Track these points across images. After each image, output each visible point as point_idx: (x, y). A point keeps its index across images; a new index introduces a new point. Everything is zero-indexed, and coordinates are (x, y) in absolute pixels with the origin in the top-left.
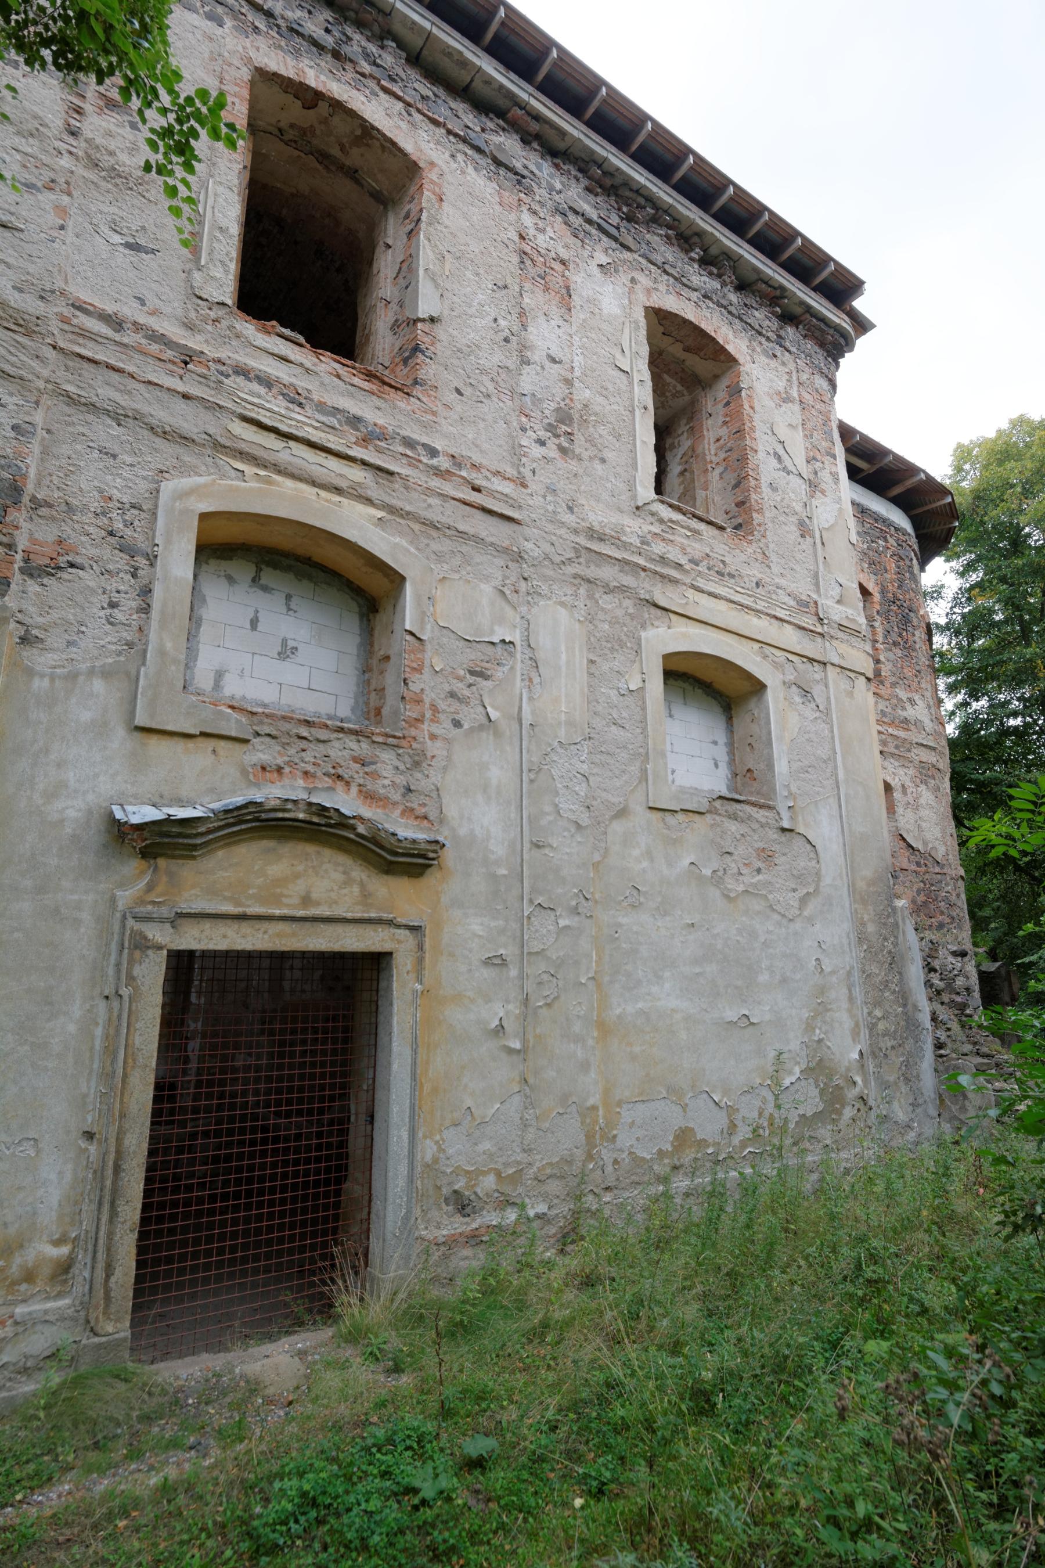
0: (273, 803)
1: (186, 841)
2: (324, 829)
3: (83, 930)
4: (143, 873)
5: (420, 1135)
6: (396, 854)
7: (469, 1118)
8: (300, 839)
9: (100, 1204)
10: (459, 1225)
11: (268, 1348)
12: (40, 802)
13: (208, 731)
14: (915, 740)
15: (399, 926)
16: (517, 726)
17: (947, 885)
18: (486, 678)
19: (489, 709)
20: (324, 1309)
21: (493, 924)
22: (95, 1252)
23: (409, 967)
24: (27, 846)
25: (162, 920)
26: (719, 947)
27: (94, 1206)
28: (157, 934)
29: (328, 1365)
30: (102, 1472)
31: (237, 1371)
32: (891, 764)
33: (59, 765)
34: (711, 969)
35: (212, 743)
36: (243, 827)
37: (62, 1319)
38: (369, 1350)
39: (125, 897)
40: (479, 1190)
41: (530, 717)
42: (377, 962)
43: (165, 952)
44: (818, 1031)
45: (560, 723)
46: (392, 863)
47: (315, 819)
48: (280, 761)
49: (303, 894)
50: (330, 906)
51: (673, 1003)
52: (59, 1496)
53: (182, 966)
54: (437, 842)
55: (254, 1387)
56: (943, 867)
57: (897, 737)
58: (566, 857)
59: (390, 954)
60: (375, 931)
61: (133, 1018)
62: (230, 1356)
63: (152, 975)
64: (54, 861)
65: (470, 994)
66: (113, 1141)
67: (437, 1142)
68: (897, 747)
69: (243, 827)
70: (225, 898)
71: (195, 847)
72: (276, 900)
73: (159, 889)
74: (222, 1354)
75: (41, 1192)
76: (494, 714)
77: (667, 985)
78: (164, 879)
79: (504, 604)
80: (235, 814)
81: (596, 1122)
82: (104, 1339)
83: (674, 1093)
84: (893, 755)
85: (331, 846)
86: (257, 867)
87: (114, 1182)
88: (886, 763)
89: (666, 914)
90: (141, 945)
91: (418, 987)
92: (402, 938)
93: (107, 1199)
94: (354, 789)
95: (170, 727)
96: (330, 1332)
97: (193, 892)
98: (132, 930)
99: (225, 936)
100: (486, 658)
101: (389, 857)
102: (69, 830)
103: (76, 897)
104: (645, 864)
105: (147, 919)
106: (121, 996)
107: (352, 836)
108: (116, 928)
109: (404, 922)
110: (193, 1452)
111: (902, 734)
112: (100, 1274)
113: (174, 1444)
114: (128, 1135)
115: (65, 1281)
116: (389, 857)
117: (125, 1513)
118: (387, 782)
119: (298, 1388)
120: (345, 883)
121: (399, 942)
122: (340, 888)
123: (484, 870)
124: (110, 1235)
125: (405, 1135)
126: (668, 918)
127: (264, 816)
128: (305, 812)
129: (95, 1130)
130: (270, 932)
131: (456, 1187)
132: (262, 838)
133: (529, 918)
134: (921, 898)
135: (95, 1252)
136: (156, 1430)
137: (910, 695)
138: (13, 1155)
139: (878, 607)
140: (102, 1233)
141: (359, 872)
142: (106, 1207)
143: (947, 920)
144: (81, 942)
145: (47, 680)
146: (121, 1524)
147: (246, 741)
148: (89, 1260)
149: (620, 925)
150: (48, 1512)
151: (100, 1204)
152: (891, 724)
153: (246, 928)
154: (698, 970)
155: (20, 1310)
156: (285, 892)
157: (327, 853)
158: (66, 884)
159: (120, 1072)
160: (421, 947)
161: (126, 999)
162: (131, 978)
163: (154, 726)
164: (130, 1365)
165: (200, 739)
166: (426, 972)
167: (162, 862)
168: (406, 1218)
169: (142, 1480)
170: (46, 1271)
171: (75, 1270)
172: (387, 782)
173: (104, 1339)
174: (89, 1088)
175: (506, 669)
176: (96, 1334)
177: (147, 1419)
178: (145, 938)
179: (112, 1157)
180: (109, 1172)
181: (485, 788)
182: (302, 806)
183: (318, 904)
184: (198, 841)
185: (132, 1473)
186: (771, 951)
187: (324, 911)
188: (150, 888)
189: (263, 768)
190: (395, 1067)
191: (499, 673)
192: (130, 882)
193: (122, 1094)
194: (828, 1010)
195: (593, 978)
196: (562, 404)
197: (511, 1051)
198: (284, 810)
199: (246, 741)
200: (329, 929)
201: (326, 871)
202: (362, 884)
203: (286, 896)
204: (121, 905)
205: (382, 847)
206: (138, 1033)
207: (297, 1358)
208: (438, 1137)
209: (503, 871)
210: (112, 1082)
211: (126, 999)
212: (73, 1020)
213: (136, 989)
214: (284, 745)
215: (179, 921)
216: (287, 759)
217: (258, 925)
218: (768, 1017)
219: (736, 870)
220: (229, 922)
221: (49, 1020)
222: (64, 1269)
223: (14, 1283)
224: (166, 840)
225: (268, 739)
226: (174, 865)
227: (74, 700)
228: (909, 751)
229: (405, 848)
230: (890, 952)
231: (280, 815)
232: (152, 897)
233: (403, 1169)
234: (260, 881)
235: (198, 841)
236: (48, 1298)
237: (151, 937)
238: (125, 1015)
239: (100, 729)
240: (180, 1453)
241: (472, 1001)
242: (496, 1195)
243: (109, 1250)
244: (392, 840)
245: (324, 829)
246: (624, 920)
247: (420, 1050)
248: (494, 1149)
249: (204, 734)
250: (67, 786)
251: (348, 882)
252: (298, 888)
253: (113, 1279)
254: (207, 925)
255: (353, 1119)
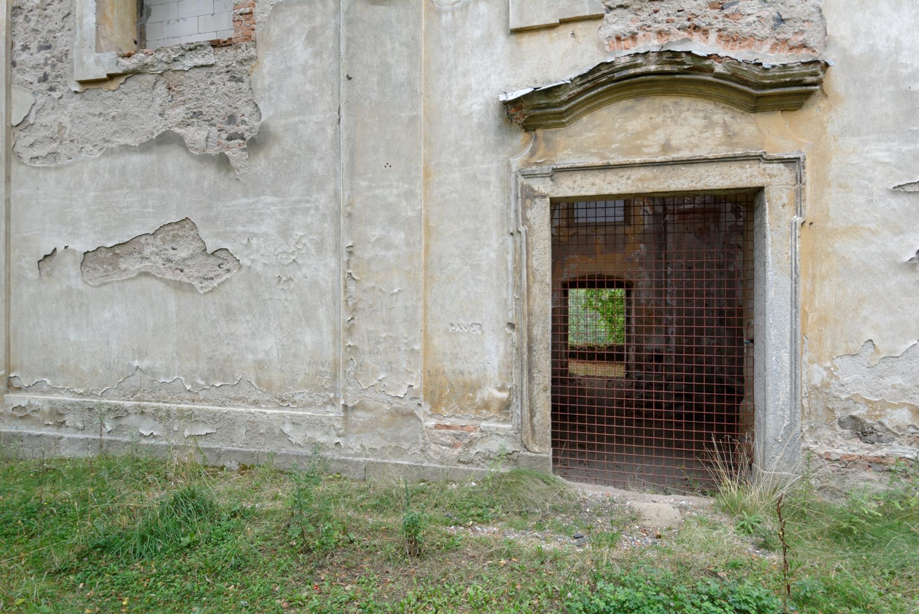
0: (624, 61)
1: (553, 110)
2: (678, 76)
3: (492, 189)
4: (527, 143)
5: (805, 358)
6: (764, 87)
7: (871, 350)
8: (656, 94)
9: (522, 370)
10: (858, 448)
11: (660, 497)
12: (456, 103)
13: (566, 17)
15: (770, 161)
20: (710, 488)
21: (905, 148)
22: (522, 400)
23: (785, 200)
24: (452, 135)
25: (543, 176)
27: (519, 371)
28: (542, 186)
29: (701, 522)
30: (518, 528)
31: (628, 503)
33: (464, 75)
35: (569, 28)
36: (600, 90)
37: (507, 435)
38: (742, 523)
39: (517, 162)
40: (886, 422)
42: (748, 201)
43: (548, 199)
46: (758, 97)
47: (667, 68)
48: (633, 28)
49: (663, 142)
50: (691, 150)
52: (488, 532)
53: (564, 210)
54: (816, 62)
55: (635, 517)
59: (760, 190)
60: (742, 168)
61: (530, 248)
62: (626, 493)
63: (540, 218)
64: (469, 143)
65: (873, 226)
66: (525, 330)
67: (827, 369)
69: (600, 90)
70: (592, 154)
71: (561, 115)
72: (638, 150)
73: (540, 153)
74: (623, 491)
75: (487, 357)
78: (543, 145)
80: (590, 78)
82: (533, 455)
85: (689, 94)
86: (617, 125)
87: (529, 357)
90: (529, 195)
91: (799, 220)
92: (775, 172)
93: (525, 367)
94: (713, 36)
95: (536, 23)
96: (712, 501)
97: (565, 152)
98: (523, 185)
99: (593, 184)
101: (754, 91)
102: (476, 120)
103: (485, 166)
105: (532, 176)
106: (520, 232)
107: (710, 78)
108: (513, 185)
109: (776, 155)
110: (575, 541)
112: (527, 415)
113: (565, 531)
114: (535, 328)
115: (507, 414)
116: (754, 91)
117: (509, 556)
118: (751, 19)
119: (670, 529)
120: (706, 127)
121: (771, 176)
122: (701, 132)
123: (891, 88)
124: (530, 391)
125: (786, 357)
127: (617, 75)
128: (656, 63)
129: (514, 322)
130: (633, 178)
131: (854, 414)
132: (619, 99)
135: (522, 400)
136: (558, 518)
138: (469, 332)
140: (524, 388)
141: (721, 115)
142: (526, 372)
144: (492, 198)
145: (450, 14)
146: (503, 561)
147: (600, 17)
148: (519, 404)
150: (478, 537)
151: (522, 370)
153: (610, 176)
155: (484, 424)
156: (645, 143)
157: (686, 101)
158: (478, 158)
159: (525, 284)
160: (799, 179)
161: (523, 234)
162: (526, 220)
163: (524, 25)
164: (552, 476)
165: (561, 27)
166: (808, 204)
167: (540, 132)
168: (790, 428)
169: (528, 541)
170: (496, 405)
171: (512, 408)
172: (751, 19)
173: (533, 455)
174: (508, 294)
176: (528, 450)
177: (555, 510)
178: (533, 190)
179: (526, 340)
180: (525, 350)
182: (653, 58)
183: (679, 149)
184: (564, 108)
185: (532, 537)
187: (685, 154)
188: (533, 153)
189: (618, 39)
190: (771, 294)
192: (519, 150)
193: (528, 300)
198: (636, 66)
199: (600, 17)
200: (691, 170)
201: (685, 119)
202: (725, 126)
203: (646, 147)
204: (514, 170)
205: (745, 83)
206: (534, 258)
207: (677, 510)
208: (828, 364)
210: (524, 294)
211: (523, 234)
212: (494, 249)
213: (530, 227)
214: (636, 12)
215: (556, 175)
216: (640, 24)
217: (621, 172)
220: (596, 172)
221: (478, 250)
222: (506, 406)
223: (478, 408)
224: (538, 112)
225: (620, 11)
226: (548, 133)
227: (468, 24)
229: (774, 77)
231: (632, 71)
232: (536, 159)
233: (785, 386)
234: (621, 136)
235: (564, 108)
236: (498, 421)
237: (536, 189)
238: (524, 245)
239: (488, 40)
240: (567, 538)
241: (874, 233)
242: (912, 430)
243: (530, 400)
244: (757, 71)
245: (678, 76)
247: (801, 280)
248: (908, 385)
249: (564, 22)
250: (471, 89)
251: (711, 125)
252: (659, 137)
253: (535, 419)
254: (578, 176)
255: (745, 351)
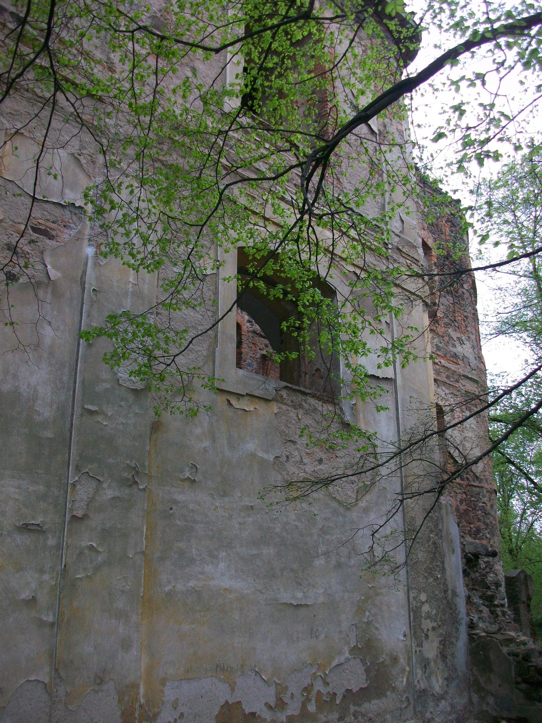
14: (462, 373)
16: (79, 289)
17: (484, 496)
18: (51, 238)
19: (49, 267)
21: (31, 488)
26: (278, 530)
32: (443, 391)
34: (269, 551)
41: (94, 283)
44: (367, 614)
45: (126, 293)
51: (226, 583)
56: (481, 481)
57: (448, 369)
58: (121, 427)
68: (448, 377)
76: (53, 274)
77: (222, 565)
79: (77, 170)
81: (137, 699)
83: (222, 670)
84: (444, 383)
88: (439, 390)
89: (225, 494)
100: (51, 218)
104: (207, 443)
111: (453, 367)
126: (226, 499)
133: (74, 485)
134: (463, 507)
137: (459, 335)
139: (435, 260)
143: (483, 526)
149: (176, 502)
152: (444, 357)
154: (255, 552)
175: (73, 232)
181: (38, 346)
186: (328, 537)
191: (66, 235)
194: (378, 594)
195: (143, 553)
196: (159, 15)
197: (41, 624)
209: (49, 434)
218: (321, 599)
219: (298, 459)
228: (457, 381)
230: (434, 543)
246: (179, 497)
